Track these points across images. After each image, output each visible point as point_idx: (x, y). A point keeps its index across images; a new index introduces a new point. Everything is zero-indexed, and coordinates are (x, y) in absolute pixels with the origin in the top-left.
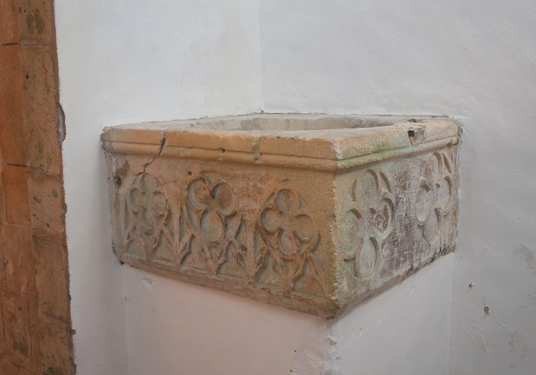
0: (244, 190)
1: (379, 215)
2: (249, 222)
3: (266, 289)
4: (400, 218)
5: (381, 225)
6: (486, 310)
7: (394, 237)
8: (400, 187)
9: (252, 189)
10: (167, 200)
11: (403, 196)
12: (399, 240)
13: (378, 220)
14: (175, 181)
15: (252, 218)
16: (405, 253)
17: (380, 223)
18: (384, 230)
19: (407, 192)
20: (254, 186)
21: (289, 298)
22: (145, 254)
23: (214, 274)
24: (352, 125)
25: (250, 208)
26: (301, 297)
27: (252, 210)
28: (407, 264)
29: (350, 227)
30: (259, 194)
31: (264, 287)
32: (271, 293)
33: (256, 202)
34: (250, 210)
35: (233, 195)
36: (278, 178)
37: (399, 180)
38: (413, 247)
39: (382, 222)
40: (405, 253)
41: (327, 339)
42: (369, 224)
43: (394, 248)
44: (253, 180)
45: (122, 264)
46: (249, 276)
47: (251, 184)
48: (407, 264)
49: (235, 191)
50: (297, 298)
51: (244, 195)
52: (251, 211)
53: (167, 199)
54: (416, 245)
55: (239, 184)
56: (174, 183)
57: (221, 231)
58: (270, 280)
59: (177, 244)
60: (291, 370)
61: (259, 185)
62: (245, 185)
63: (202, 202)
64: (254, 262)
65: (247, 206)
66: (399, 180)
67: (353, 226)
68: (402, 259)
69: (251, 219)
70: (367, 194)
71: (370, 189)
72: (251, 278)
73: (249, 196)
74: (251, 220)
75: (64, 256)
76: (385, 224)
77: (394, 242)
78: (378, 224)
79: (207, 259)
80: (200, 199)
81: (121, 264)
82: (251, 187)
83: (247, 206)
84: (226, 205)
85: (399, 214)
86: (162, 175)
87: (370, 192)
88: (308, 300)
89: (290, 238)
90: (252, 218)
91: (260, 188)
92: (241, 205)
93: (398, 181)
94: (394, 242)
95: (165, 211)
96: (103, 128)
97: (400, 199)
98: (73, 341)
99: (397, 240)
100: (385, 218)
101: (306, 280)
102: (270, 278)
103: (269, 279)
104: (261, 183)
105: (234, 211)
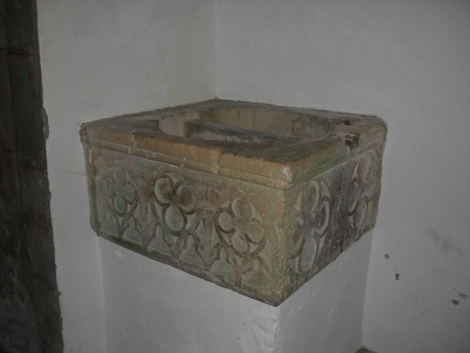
0: (203, 193)
1: (318, 215)
2: (207, 221)
3: (220, 277)
4: (335, 214)
5: (319, 223)
6: (397, 276)
7: (329, 231)
8: (337, 188)
9: (210, 193)
10: (136, 192)
11: (338, 196)
12: (333, 233)
13: (318, 219)
14: (143, 177)
15: (209, 217)
16: (337, 241)
17: (318, 222)
18: (321, 226)
19: (341, 192)
20: (212, 191)
21: (240, 287)
22: (117, 232)
23: (176, 258)
24: (293, 119)
25: (208, 209)
26: (250, 288)
27: (210, 211)
28: (338, 250)
29: (295, 230)
30: (216, 198)
31: (219, 275)
32: (225, 281)
33: (214, 205)
34: (208, 211)
35: (193, 196)
36: (233, 188)
37: (336, 183)
38: (344, 235)
39: (321, 220)
40: (337, 241)
41: (271, 318)
42: (310, 225)
43: (329, 240)
44: (211, 186)
45: (98, 236)
46: (206, 264)
47: (210, 189)
48: (338, 250)
49: (196, 193)
50: (247, 289)
51: (203, 198)
52: (208, 212)
53: (136, 191)
54: (346, 232)
55: (199, 187)
56: (142, 179)
57: (182, 223)
58: (224, 269)
59: (144, 229)
60: (239, 339)
61: (216, 191)
62: (204, 190)
63: (166, 197)
64: (210, 253)
65: (205, 207)
66: (336, 183)
67: (297, 230)
68: (335, 247)
69: (208, 218)
70: (310, 200)
71: (312, 195)
72: (207, 266)
73: (207, 199)
74: (209, 220)
75: (49, 211)
76: (323, 222)
77: (329, 235)
78: (317, 223)
79: (170, 245)
80: (164, 194)
81: (97, 236)
82: (209, 191)
83: (205, 207)
84: (187, 203)
85: (335, 211)
86: (131, 170)
87: (312, 198)
88: (256, 291)
89: (242, 238)
90: (209, 217)
91: (217, 194)
92: (200, 205)
93: (335, 184)
94: (329, 235)
95: (135, 201)
96: (81, 123)
97: (336, 199)
98: (59, 300)
99: (332, 233)
100: (323, 217)
101: (255, 275)
102: (224, 268)
103: (223, 269)
104: (219, 190)
105: (194, 209)
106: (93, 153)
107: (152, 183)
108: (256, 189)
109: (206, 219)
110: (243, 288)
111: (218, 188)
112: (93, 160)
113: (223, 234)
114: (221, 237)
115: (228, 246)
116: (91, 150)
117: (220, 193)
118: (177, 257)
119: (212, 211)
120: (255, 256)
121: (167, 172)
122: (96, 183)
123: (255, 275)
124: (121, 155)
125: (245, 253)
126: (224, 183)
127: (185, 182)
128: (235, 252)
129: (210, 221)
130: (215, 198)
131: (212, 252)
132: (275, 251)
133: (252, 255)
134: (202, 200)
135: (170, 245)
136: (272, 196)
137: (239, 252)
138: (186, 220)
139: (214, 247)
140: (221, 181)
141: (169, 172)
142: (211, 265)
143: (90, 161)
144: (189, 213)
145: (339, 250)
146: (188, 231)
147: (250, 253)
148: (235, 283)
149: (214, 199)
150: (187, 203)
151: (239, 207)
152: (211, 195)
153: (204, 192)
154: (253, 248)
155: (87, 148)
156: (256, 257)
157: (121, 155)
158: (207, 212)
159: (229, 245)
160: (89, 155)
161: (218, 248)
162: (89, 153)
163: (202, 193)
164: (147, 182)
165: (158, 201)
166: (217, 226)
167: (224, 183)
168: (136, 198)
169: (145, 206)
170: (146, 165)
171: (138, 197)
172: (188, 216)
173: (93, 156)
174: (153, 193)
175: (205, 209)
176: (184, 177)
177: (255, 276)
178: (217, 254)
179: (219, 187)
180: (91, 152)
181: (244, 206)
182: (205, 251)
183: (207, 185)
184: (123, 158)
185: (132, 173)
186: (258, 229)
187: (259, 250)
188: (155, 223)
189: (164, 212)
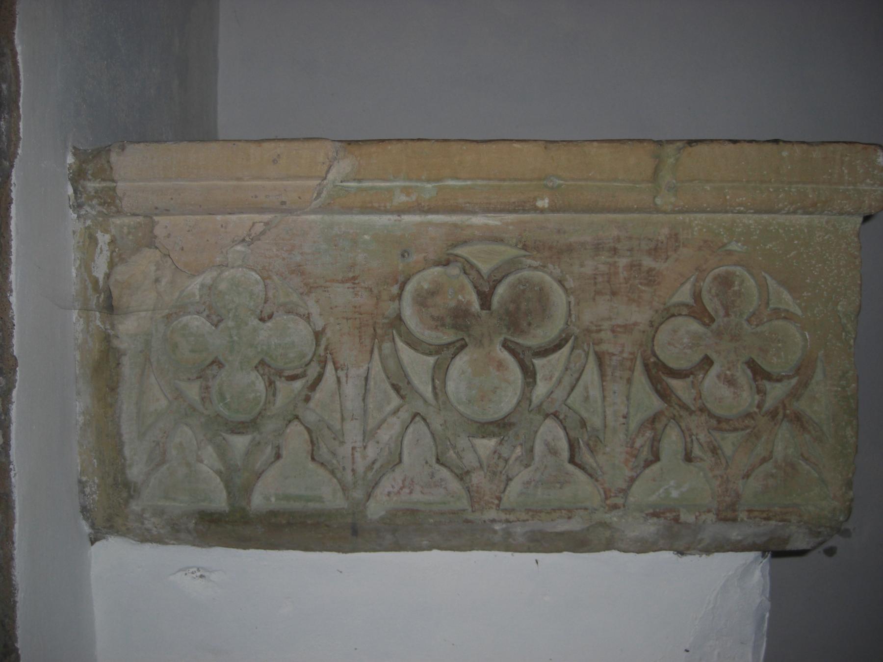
0: (600, 279)
2: (614, 358)
14: (354, 278)
15: (623, 346)
27: (625, 326)
34: (619, 326)
47: (623, 262)
51: (598, 293)
62: (603, 268)
63: (443, 325)
64: (627, 453)
72: (616, 496)
74: (622, 352)
82: (620, 270)
89: (728, 382)
92: (587, 317)
95: (313, 364)
102: (666, 487)
106: (113, 242)
107: (395, 289)
108: (781, 231)
109: (609, 353)
110: (742, 520)
111: (655, 251)
112: (112, 265)
113: (676, 384)
114: (664, 394)
115: (691, 413)
116: (106, 231)
117: (659, 265)
118: (496, 502)
119: (635, 324)
120: (780, 416)
121: (454, 246)
122: (123, 344)
123: (774, 471)
124: (254, 224)
125: (749, 415)
126: (675, 237)
127: (529, 261)
128: (714, 422)
129: (625, 355)
130: (641, 284)
131: (632, 447)
132: (843, 383)
133: (773, 415)
134: (594, 299)
135: (468, 472)
136: (830, 237)
137: (728, 420)
138: (529, 374)
139: (642, 427)
140: (665, 231)
141: (465, 242)
142: (629, 487)
143: (100, 270)
144: (544, 352)
145: (19, 627)
146: (540, 406)
147: (764, 410)
148: (717, 515)
149: (639, 286)
150: (530, 324)
151: (717, 295)
152: (627, 280)
153: (603, 275)
154: (776, 392)
155: (88, 228)
156: (785, 416)
157: (254, 224)
158: (613, 331)
159: (693, 408)
160: (98, 250)
161: (653, 429)
162: (97, 244)
163: (595, 278)
164: (371, 290)
165: (414, 344)
166: (654, 363)
167: (675, 237)
168: (321, 351)
169: (362, 371)
170: (366, 237)
171: (326, 349)
172: (538, 362)
173: (113, 252)
174: (399, 318)
175: (606, 325)
176: (525, 247)
177: (772, 475)
178: (652, 446)
179: (656, 249)
180: (103, 239)
181: (736, 288)
182: (608, 449)
183: (615, 251)
184: (263, 233)
185: (303, 273)
186: (779, 341)
187: (794, 394)
188: (404, 415)
189: (440, 373)
